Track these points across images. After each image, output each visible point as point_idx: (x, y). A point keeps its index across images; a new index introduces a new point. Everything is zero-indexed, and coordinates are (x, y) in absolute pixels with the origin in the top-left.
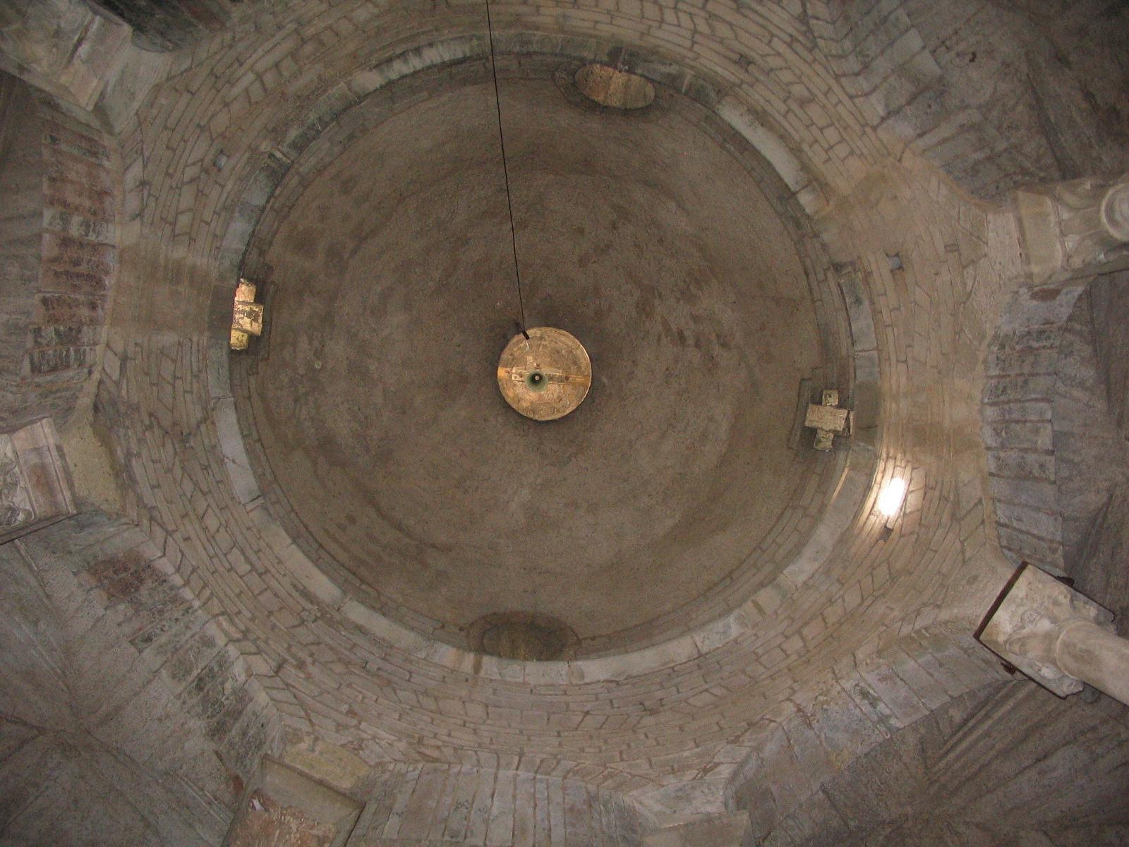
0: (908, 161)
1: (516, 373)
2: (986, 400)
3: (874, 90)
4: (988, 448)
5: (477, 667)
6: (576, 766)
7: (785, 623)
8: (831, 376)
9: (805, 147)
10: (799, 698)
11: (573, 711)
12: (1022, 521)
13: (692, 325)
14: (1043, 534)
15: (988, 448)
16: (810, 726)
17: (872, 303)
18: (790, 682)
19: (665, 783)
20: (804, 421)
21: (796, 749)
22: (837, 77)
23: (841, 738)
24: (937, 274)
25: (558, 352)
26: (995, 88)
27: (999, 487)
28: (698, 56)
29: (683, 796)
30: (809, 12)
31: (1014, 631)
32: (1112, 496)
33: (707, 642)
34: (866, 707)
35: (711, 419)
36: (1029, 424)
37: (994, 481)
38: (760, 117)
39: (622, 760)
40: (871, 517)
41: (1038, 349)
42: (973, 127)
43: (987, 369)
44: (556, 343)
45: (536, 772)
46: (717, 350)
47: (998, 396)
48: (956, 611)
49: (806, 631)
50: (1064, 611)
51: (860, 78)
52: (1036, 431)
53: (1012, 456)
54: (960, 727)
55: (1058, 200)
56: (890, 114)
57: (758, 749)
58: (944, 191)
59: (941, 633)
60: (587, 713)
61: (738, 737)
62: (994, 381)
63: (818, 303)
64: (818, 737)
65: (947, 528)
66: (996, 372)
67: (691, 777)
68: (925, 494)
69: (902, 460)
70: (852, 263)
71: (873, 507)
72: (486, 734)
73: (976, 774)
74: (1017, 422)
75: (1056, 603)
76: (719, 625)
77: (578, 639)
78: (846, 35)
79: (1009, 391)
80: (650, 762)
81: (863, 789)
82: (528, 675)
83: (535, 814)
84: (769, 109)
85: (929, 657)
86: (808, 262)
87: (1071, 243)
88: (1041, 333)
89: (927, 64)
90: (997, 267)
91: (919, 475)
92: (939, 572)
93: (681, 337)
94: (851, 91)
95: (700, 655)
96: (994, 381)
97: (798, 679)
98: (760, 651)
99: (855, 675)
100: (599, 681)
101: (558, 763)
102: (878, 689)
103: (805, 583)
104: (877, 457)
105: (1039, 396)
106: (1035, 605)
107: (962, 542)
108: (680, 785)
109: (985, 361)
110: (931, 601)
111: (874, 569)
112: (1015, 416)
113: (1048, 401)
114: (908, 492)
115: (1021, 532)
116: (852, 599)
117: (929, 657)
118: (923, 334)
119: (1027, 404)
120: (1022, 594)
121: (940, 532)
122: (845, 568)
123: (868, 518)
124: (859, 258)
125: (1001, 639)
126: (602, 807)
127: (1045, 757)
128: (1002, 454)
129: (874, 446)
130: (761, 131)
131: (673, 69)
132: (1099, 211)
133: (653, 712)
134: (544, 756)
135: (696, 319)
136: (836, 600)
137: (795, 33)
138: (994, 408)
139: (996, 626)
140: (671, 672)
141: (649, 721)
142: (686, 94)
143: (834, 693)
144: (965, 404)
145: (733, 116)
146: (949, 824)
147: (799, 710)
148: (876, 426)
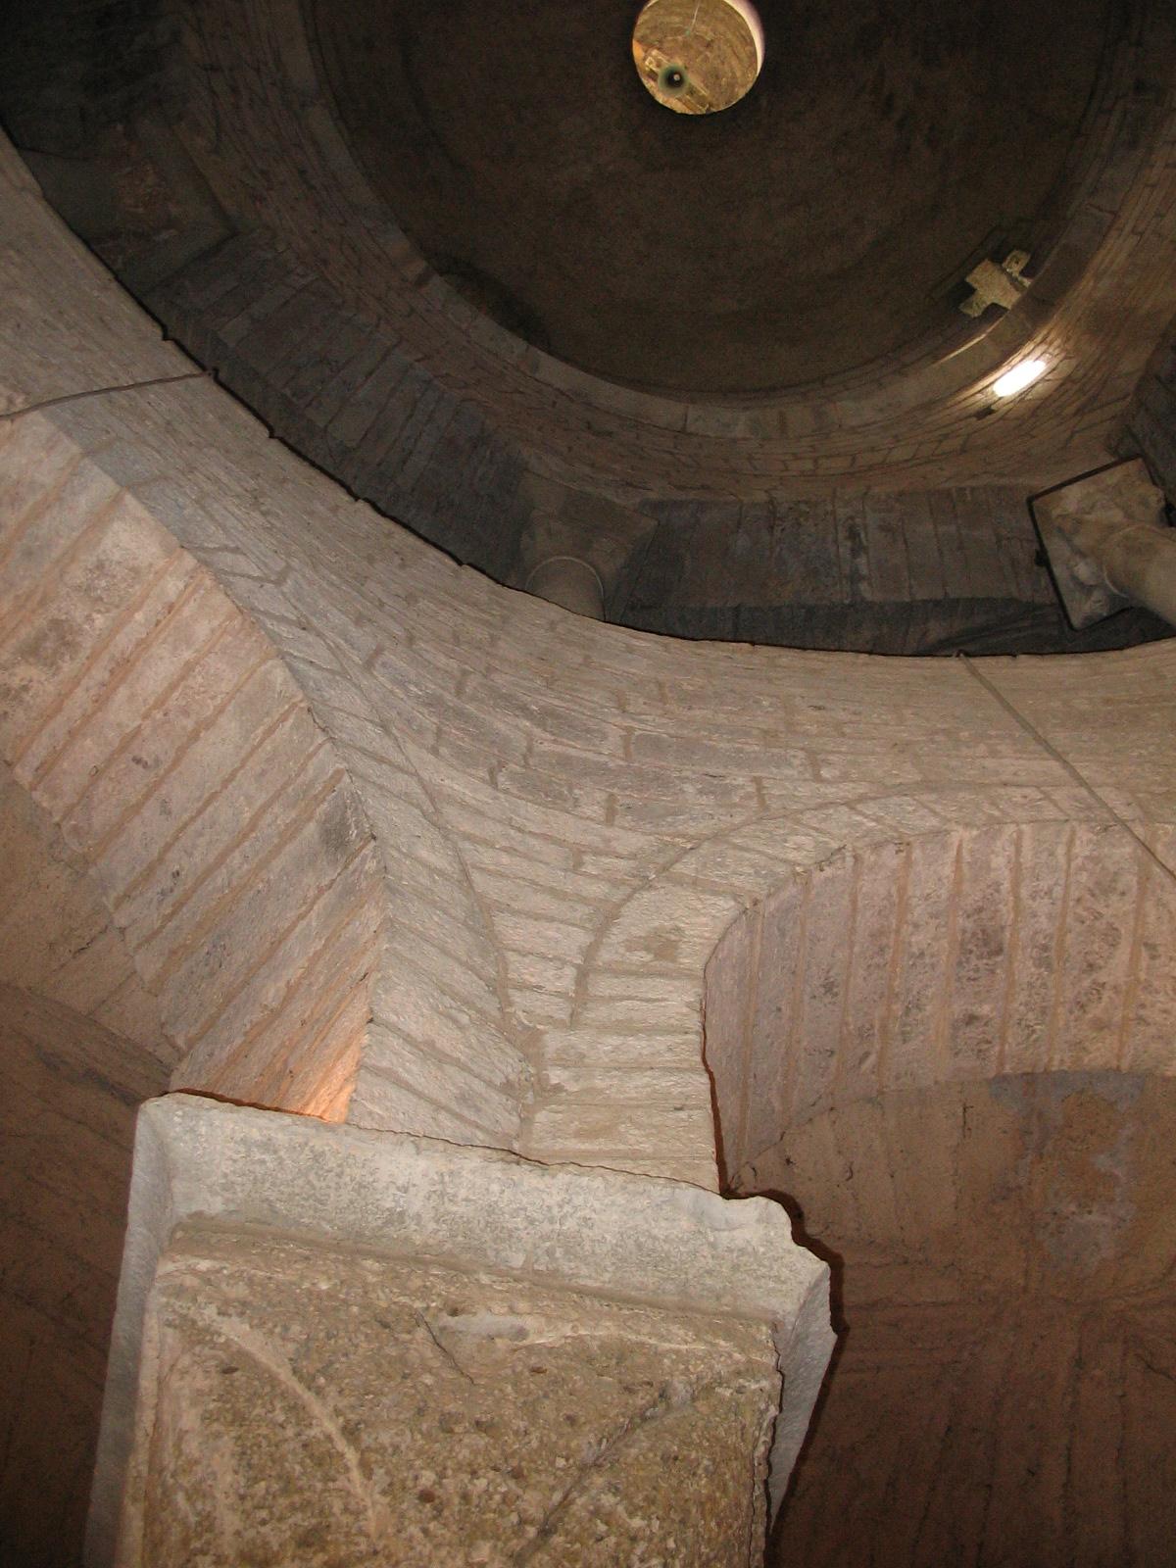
1: (654, 57)
5: (421, 281)
25: (717, 77)
34: (844, 551)
44: (723, 63)
71: (987, 386)
85: (953, 528)
95: (683, 431)
104: (1029, 337)
114: (1042, 380)
117: (953, 528)
118: (1002, 791)
125: (1055, 513)
126: (488, 453)
139: (1061, 498)
148: (1053, 305)
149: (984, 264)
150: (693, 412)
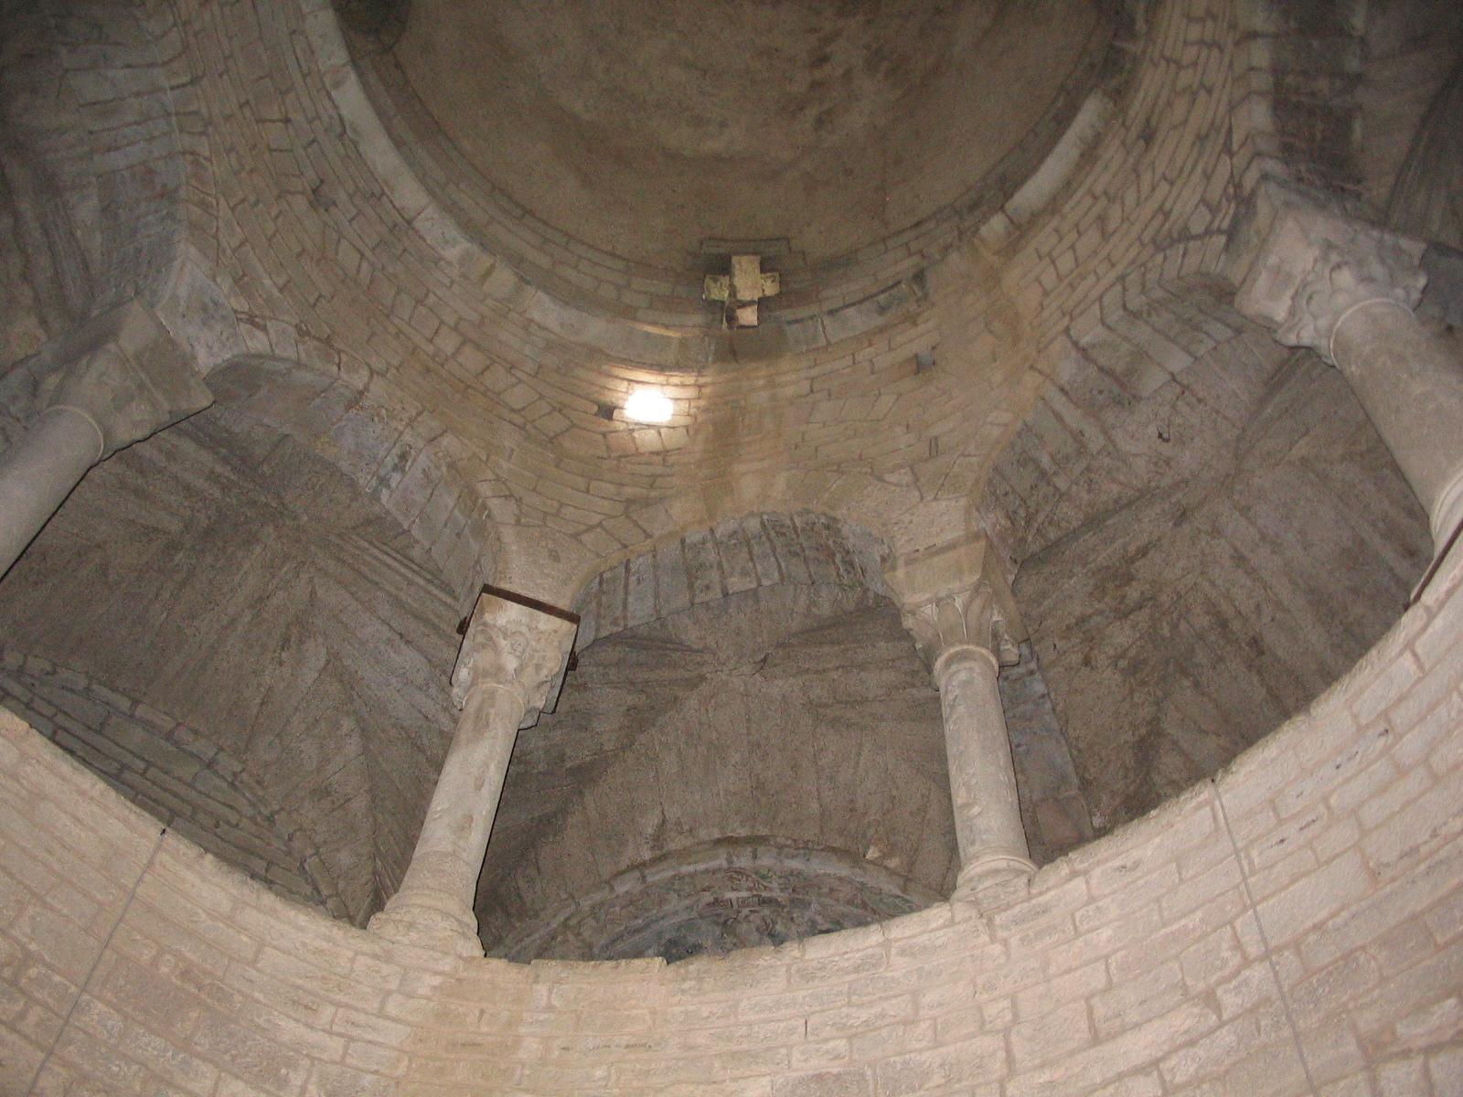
0: (1031, 379)
2: (765, 517)
3: (1109, 328)
4: (712, 531)
6: (205, 158)
7: (474, 316)
8: (799, 278)
9: (1055, 222)
10: (378, 387)
11: (284, 102)
12: (639, 583)
13: (840, 71)
14: (630, 608)
15: (712, 531)
16: (348, 407)
17: (882, 330)
18: (395, 362)
19: (219, 280)
20: (737, 254)
21: (318, 401)
22: (1122, 278)
23: (349, 441)
24: (908, 427)
26: (1137, 455)
27: (671, 551)
28: (1156, 65)
29: (207, 311)
30: (1191, 244)
31: (499, 629)
32: (702, 652)
33: (428, 224)
34: (391, 461)
35: (723, 125)
36: (751, 565)
37: (677, 543)
38: (1089, 154)
39: (233, 209)
40: (626, 383)
41: (834, 563)
42: (1082, 448)
43: (800, 514)
45: (177, 114)
46: (813, 112)
47: (773, 528)
48: (514, 548)
49: (468, 349)
50: (529, 677)
51: (1121, 312)
52: (744, 573)
53: (710, 555)
54: (406, 557)
55: (977, 592)
56: (1084, 352)
57: (298, 364)
58: (996, 432)
59: (489, 534)
60: (287, 121)
61: (308, 333)
62: (788, 522)
63: (881, 247)
64: (340, 420)
65: (617, 498)
66: (798, 521)
67: (237, 307)
68: (658, 453)
69: (698, 408)
70: (926, 296)
72: (207, 16)
73: (366, 578)
74: (750, 552)
75: (538, 668)
76: (453, 232)
77: (391, 48)
78: (1168, 291)
79: (782, 539)
80: (242, 244)
81: (306, 471)
82: (316, 17)
83: (129, 125)
84: (1100, 164)
86: (932, 225)
87: (930, 611)
88: (851, 564)
89: (1152, 380)
90: (907, 518)
91: (679, 438)
92: (562, 505)
93: (822, 60)
94: (1106, 300)
95: (409, 222)
96: (788, 522)
97: (401, 370)
98: (432, 299)
99: (421, 444)
100: (336, 107)
101: (201, 134)
102: (415, 471)
103: (532, 321)
105: (785, 570)
106: (533, 643)
107: (600, 525)
108: (222, 300)
109: (808, 512)
110: (525, 509)
111: (560, 411)
112: (756, 550)
113: (782, 579)
114: (657, 428)
115: (626, 586)
116: (518, 397)
119: (773, 559)
120: (542, 626)
121: (612, 488)
122: (558, 370)
123: (624, 379)
124: (933, 305)
125: (488, 617)
127: (408, 642)
128: (709, 545)
129: (714, 362)
130: (1074, 154)
131: (1140, 25)
132: (961, 642)
133: (314, 205)
134: (204, 110)
135: (848, 75)
136: (514, 375)
137: (1173, 218)
138: (758, 526)
140: (376, 194)
141: (300, 204)
142: (1112, 47)
143: (394, 424)
144: (761, 487)
145: (1090, 113)
146: (304, 563)
147: (361, 393)
149: (752, 257)
150: (431, 211)
